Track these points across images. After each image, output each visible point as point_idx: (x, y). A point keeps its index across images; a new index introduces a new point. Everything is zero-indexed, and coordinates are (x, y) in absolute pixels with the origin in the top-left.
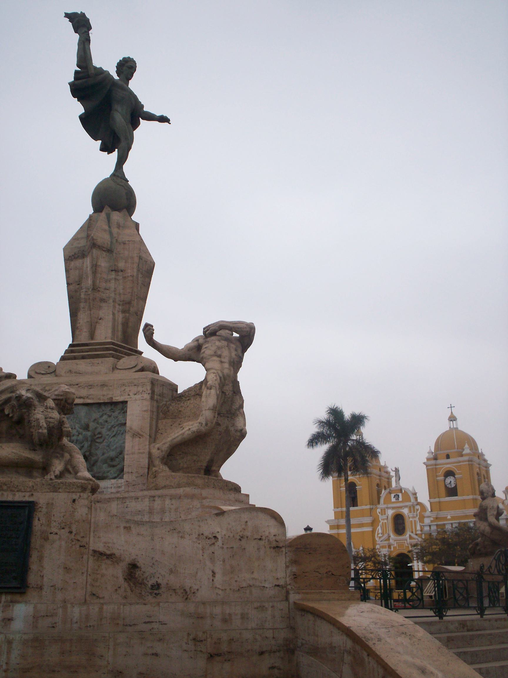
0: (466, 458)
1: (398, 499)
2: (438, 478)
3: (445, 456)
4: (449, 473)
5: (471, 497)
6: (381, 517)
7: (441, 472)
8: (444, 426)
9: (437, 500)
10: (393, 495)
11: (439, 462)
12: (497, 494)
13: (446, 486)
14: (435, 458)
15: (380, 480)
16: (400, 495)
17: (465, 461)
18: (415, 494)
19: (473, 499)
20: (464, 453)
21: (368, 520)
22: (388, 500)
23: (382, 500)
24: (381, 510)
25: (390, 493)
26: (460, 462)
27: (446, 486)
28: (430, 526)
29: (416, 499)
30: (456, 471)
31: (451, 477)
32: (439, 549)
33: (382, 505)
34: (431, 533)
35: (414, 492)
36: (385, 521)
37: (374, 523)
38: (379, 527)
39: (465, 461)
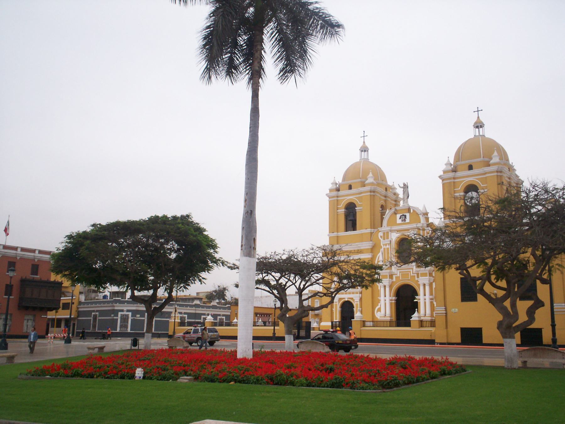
0: (368, 188)
1: (405, 220)
4: (472, 188)
6: (382, 242)
9: (335, 234)
10: (398, 216)
11: (459, 174)
14: (454, 170)
15: (385, 201)
16: (408, 215)
18: (426, 214)
21: (367, 245)
22: (392, 222)
23: (385, 222)
24: (384, 233)
29: (427, 219)
30: (480, 185)
33: (385, 227)
35: (424, 211)
36: (388, 246)
37: (374, 249)
38: (380, 254)
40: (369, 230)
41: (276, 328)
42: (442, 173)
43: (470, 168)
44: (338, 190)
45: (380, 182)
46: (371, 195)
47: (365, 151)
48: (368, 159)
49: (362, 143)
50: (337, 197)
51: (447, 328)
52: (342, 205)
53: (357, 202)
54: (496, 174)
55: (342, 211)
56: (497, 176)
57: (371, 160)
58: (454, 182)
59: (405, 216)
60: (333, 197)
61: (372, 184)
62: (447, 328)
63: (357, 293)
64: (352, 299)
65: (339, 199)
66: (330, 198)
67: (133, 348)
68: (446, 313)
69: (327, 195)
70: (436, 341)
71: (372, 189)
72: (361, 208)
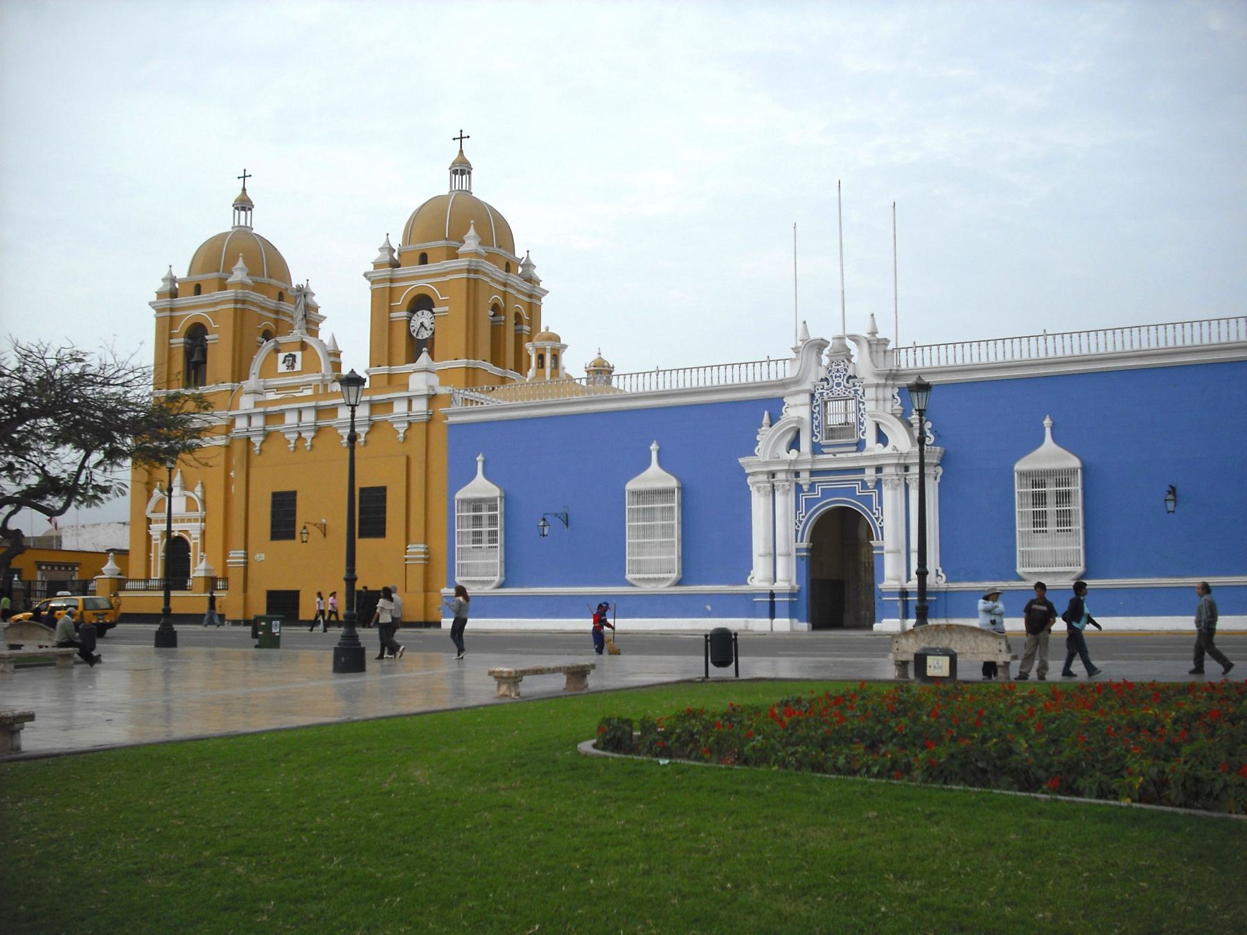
0: (462, 263)
1: (293, 366)
2: (393, 315)
3: (417, 257)
4: (422, 302)
5: (462, 363)
7: (402, 300)
8: (223, 222)
9: (384, 369)
10: (281, 356)
12: (566, 359)
13: (409, 334)
16: (299, 354)
17: (460, 271)
18: (337, 354)
19: (467, 368)
20: (462, 249)
22: (268, 370)
23: (255, 368)
25: (277, 351)
26: (444, 274)
27: (409, 334)
28: (249, 417)
29: (337, 366)
30: (438, 296)
31: (426, 312)
32: (123, 437)
33: (252, 382)
34: (249, 438)
35: (331, 348)
39: (460, 271)
40: (228, 386)
41: (173, 594)
42: (371, 268)
43: (424, 259)
44: (174, 294)
45: (495, 249)
46: (236, 309)
47: (244, 209)
48: (469, 192)
49: (240, 192)
50: (392, 280)
51: (245, 590)
52: (181, 328)
53: (211, 324)
54: (465, 275)
55: (179, 341)
56: (468, 279)
57: (477, 193)
58: (391, 289)
59: (294, 357)
60: (163, 310)
61: (243, 285)
62: (245, 590)
63: (196, 520)
64: (186, 532)
65: (395, 285)
66: (158, 311)
67: (716, 672)
68: (246, 563)
69: (365, 275)
70: (228, 617)
71: (240, 296)
72: (446, 309)
